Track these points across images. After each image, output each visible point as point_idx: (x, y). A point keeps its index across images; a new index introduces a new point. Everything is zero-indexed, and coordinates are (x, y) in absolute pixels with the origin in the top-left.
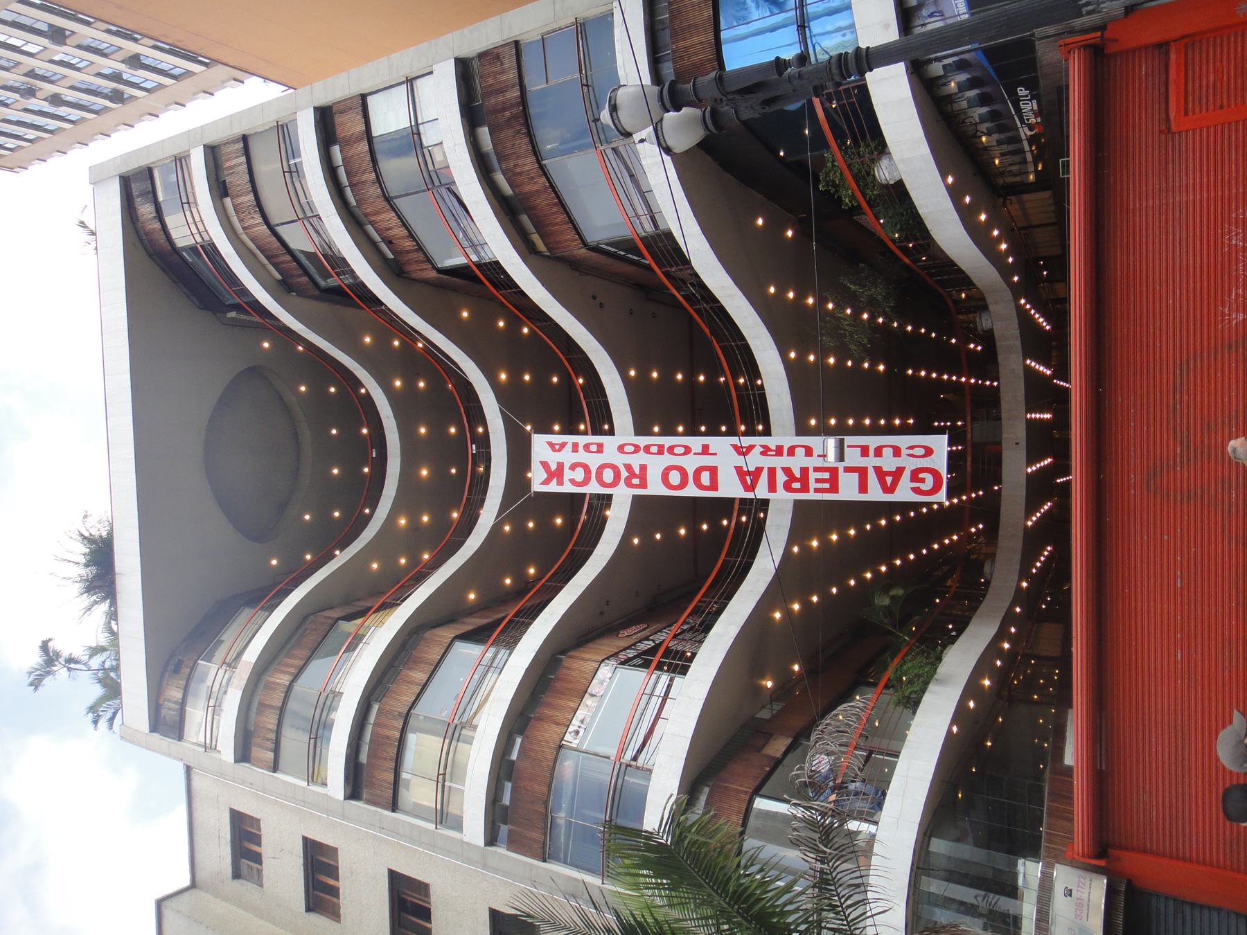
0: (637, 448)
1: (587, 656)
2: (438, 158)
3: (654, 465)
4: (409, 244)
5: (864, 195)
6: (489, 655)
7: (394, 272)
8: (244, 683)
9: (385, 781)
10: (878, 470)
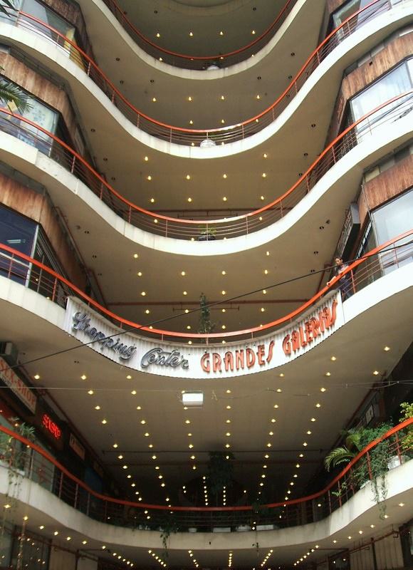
7: (348, 66)
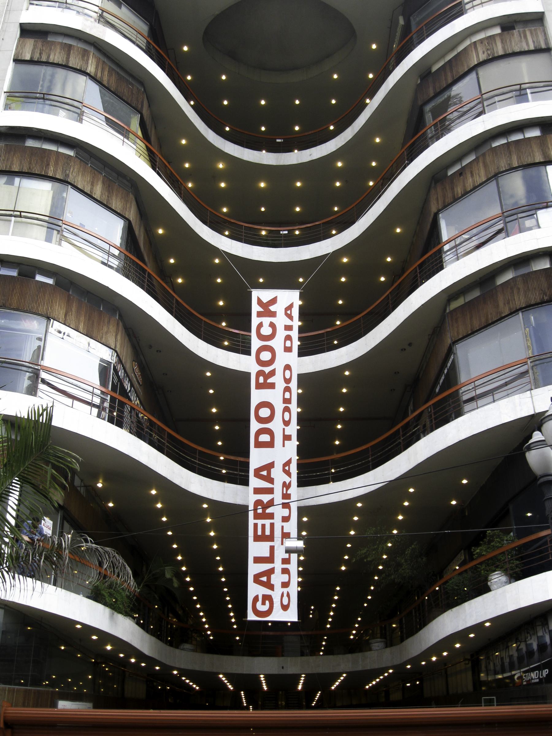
0: (288, 381)
1: (119, 337)
2: (529, 223)
3: (274, 396)
4: (459, 190)
5: (481, 564)
6: (116, 252)
7: (436, 174)
8: (88, 31)
9: (12, 163)
10: (272, 571)
